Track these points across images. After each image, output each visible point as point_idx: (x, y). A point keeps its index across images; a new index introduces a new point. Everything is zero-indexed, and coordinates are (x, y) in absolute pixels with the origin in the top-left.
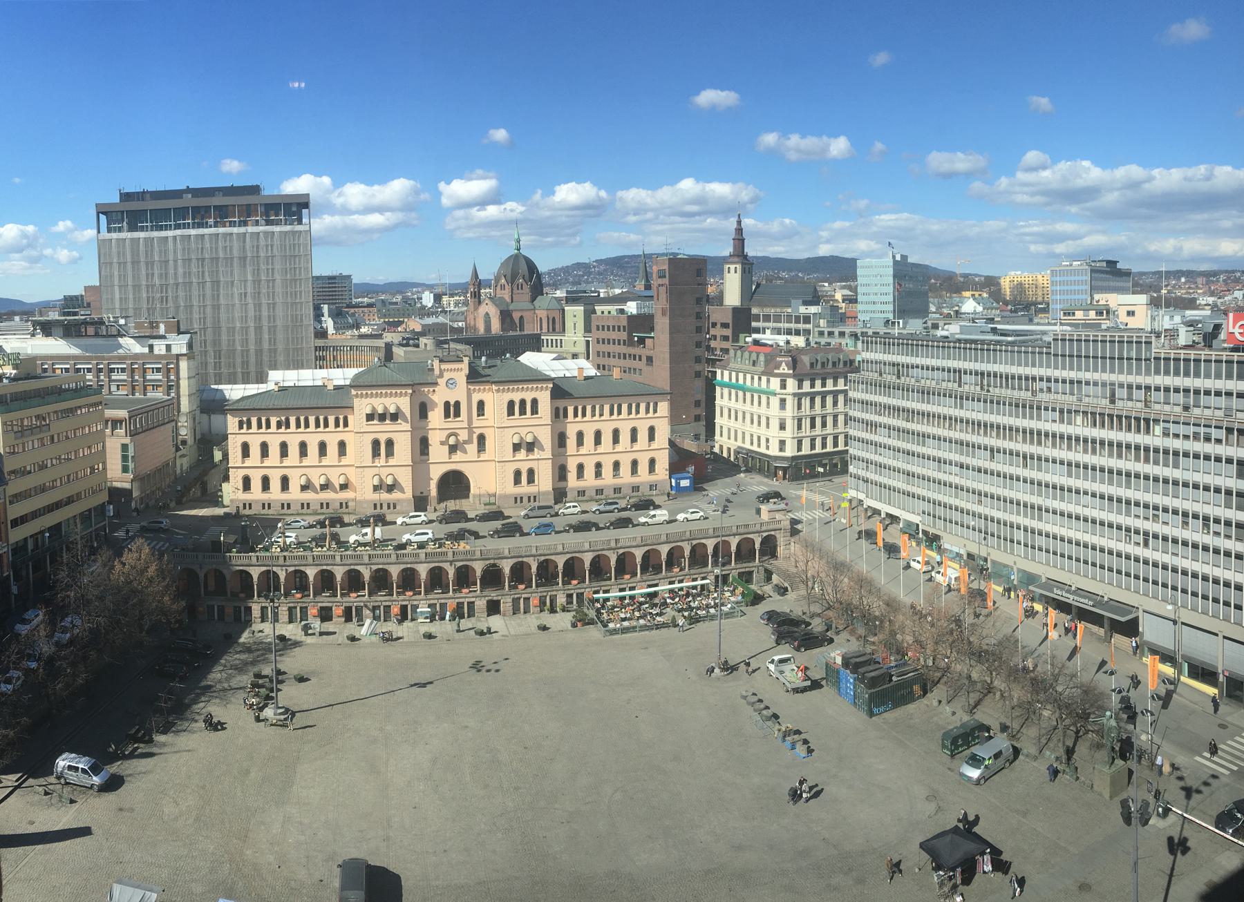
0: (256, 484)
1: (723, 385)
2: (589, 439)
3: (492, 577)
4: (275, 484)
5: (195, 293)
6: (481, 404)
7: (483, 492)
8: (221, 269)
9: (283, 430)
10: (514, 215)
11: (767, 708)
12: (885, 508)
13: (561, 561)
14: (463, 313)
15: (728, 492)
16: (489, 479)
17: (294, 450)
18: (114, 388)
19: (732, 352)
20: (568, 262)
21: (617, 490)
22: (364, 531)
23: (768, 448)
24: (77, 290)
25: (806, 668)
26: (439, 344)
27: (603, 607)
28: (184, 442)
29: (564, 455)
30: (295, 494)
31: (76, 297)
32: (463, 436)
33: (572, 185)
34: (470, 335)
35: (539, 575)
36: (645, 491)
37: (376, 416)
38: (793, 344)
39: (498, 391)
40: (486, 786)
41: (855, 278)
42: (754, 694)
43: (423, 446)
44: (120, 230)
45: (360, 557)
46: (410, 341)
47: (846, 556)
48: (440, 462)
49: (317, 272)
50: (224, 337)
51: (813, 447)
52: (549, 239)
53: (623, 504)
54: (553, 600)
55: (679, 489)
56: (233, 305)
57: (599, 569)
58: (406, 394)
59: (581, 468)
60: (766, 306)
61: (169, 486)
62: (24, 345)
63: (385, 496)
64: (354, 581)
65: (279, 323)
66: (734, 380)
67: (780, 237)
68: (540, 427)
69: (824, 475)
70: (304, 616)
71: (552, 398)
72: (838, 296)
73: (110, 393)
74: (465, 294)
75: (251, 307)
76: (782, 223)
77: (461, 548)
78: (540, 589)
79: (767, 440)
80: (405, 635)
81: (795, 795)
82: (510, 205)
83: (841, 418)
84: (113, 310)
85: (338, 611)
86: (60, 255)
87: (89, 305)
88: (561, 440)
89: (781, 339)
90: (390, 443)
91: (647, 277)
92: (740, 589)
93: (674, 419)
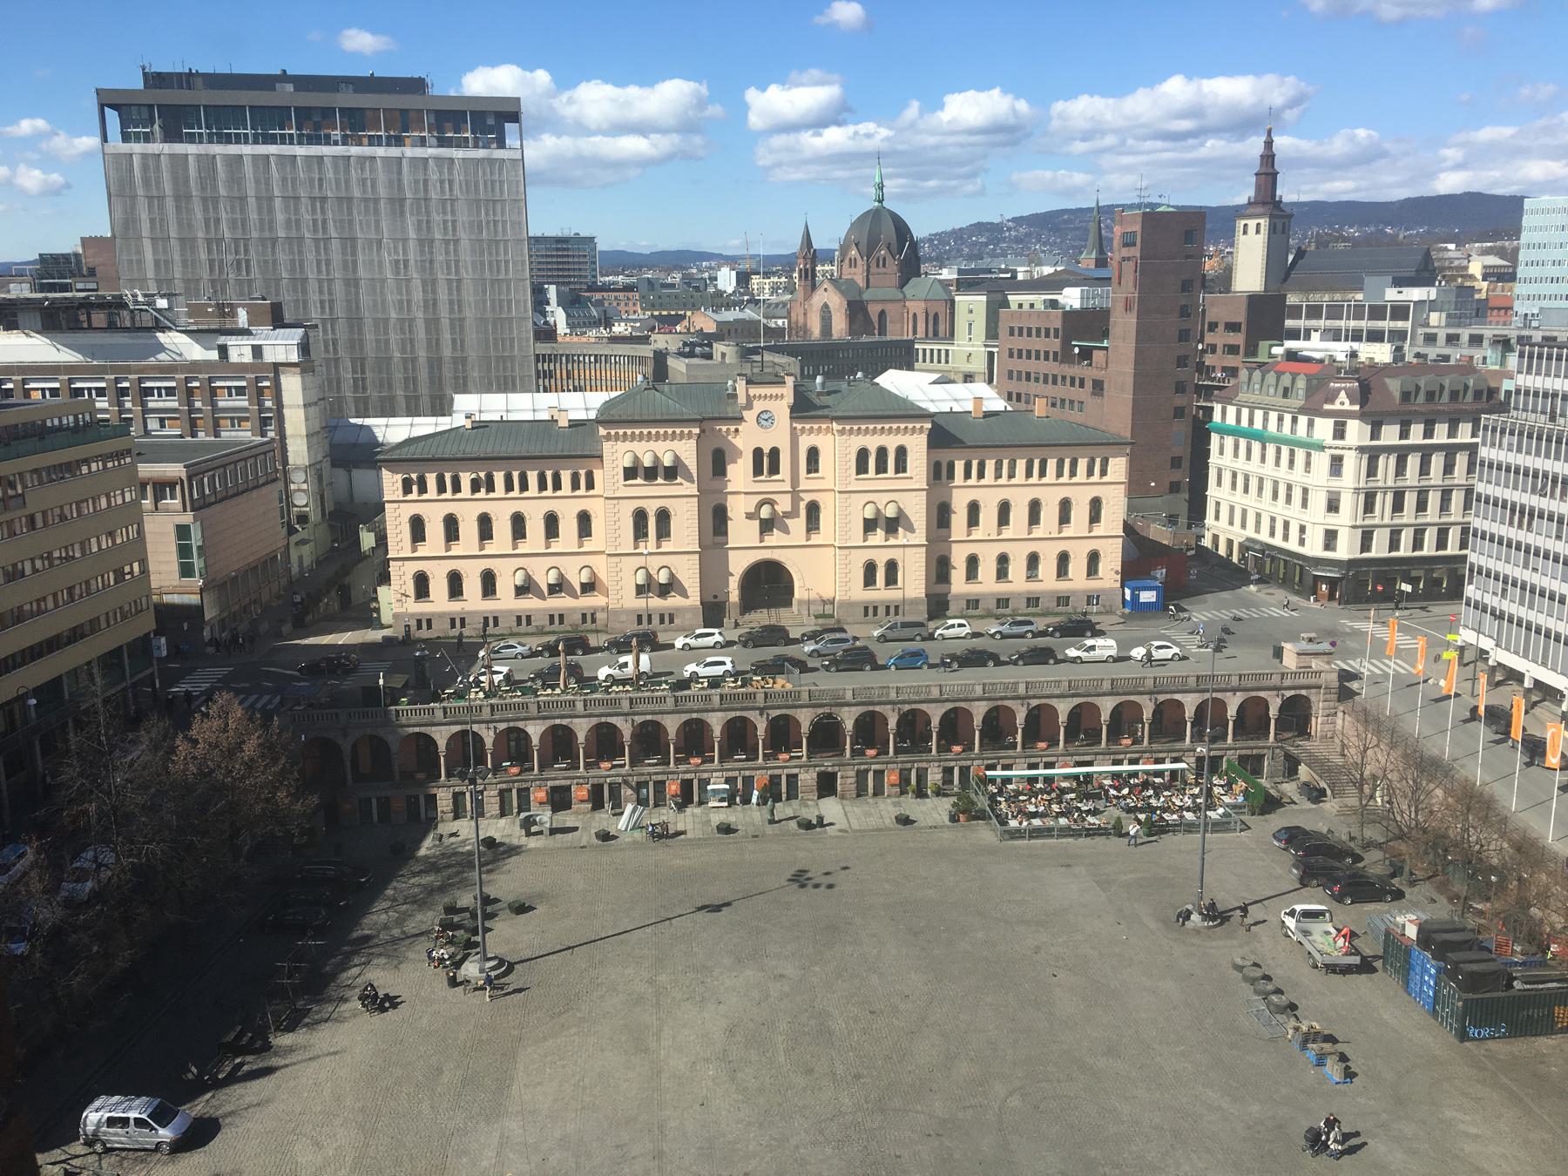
1: (1224, 431)
2: (989, 516)
3: (826, 736)
4: (472, 586)
5: (310, 256)
6: (813, 454)
7: (813, 596)
8: (357, 218)
9: (482, 494)
11: (1279, 991)
13: (936, 714)
14: (784, 304)
15: (1225, 615)
16: (824, 574)
17: (502, 528)
18: (153, 425)
19: (1243, 374)
21: (1033, 601)
22: (622, 660)
23: (1302, 542)
24: (67, 244)
25: (1353, 935)
26: (745, 354)
27: (1000, 793)
28: (303, 519)
29: (946, 540)
30: (506, 600)
31: (66, 257)
32: (784, 504)
33: (971, 93)
34: (797, 341)
35: (900, 736)
37: (641, 472)
38: (1362, 357)
39: (842, 432)
41: (1516, 232)
43: (716, 520)
44: (147, 138)
45: (616, 702)
46: (698, 347)
47: (1445, 747)
48: (745, 546)
49: (535, 230)
50: (369, 336)
52: (932, 183)
53: (1040, 624)
56: (383, 281)
57: (997, 729)
58: (690, 435)
59: (973, 562)
60: (1315, 290)
63: (656, 602)
64: (605, 742)
66: (1245, 423)
67: (1335, 164)
70: (524, 804)
71: (929, 447)
72: (1475, 268)
73: (147, 433)
77: (778, 687)
78: (901, 758)
79: (1302, 529)
80: (689, 827)
81: (1316, 1141)
83: (1457, 498)
84: (142, 283)
85: (580, 792)
88: (941, 515)
89: (1340, 350)
90: (664, 516)
92: (1241, 785)
93: (1136, 487)
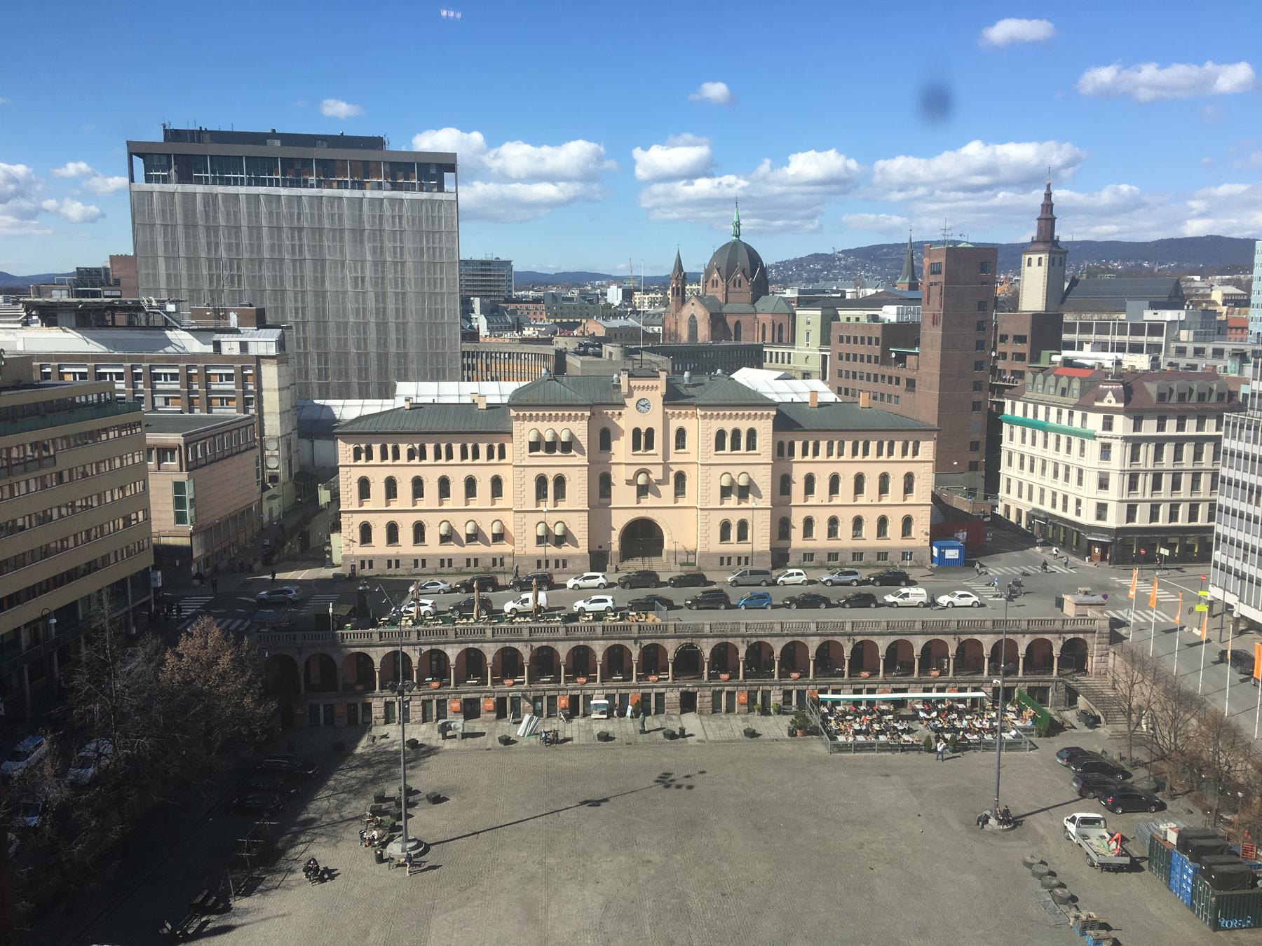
0: (379, 535)
1: (1013, 422)
2: (822, 486)
3: (688, 662)
4: (406, 534)
5: (288, 273)
6: (681, 434)
7: (679, 548)
9: (416, 461)
10: (732, 192)
11: (1062, 886)
13: (778, 646)
14: (660, 315)
16: (688, 530)
17: (431, 489)
18: (159, 402)
19: (1029, 376)
21: (858, 555)
22: (524, 596)
23: (1078, 513)
24: (99, 260)
26: (628, 353)
27: (831, 713)
28: (274, 478)
31: (97, 271)
32: (657, 473)
34: (670, 343)
36: (896, 562)
37: (543, 445)
38: (1126, 365)
39: (704, 417)
41: (1249, 268)
42: (1042, 862)
43: (602, 486)
44: (165, 180)
45: (519, 630)
46: (591, 347)
48: (625, 507)
50: (332, 335)
51: (1154, 516)
52: (779, 223)
53: (863, 574)
54: (766, 697)
55: (942, 562)
56: (345, 293)
58: (583, 417)
59: (809, 523)
61: (253, 540)
62: (10, 338)
63: (552, 550)
64: (509, 664)
66: (1030, 415)
68: (757, 467)
73: (154, 409)
76: (1117, 192)
77: (649, 621)
78: (749, 682)
79: (1078, 502)
82: (728, 179)
84: (156, 291)
86: (83, 214)
87: (117, 283)
88: (783, 484)
89: (1107, 359)
91: (914, 273)
92: (1030, 711)
93: (942, 466)
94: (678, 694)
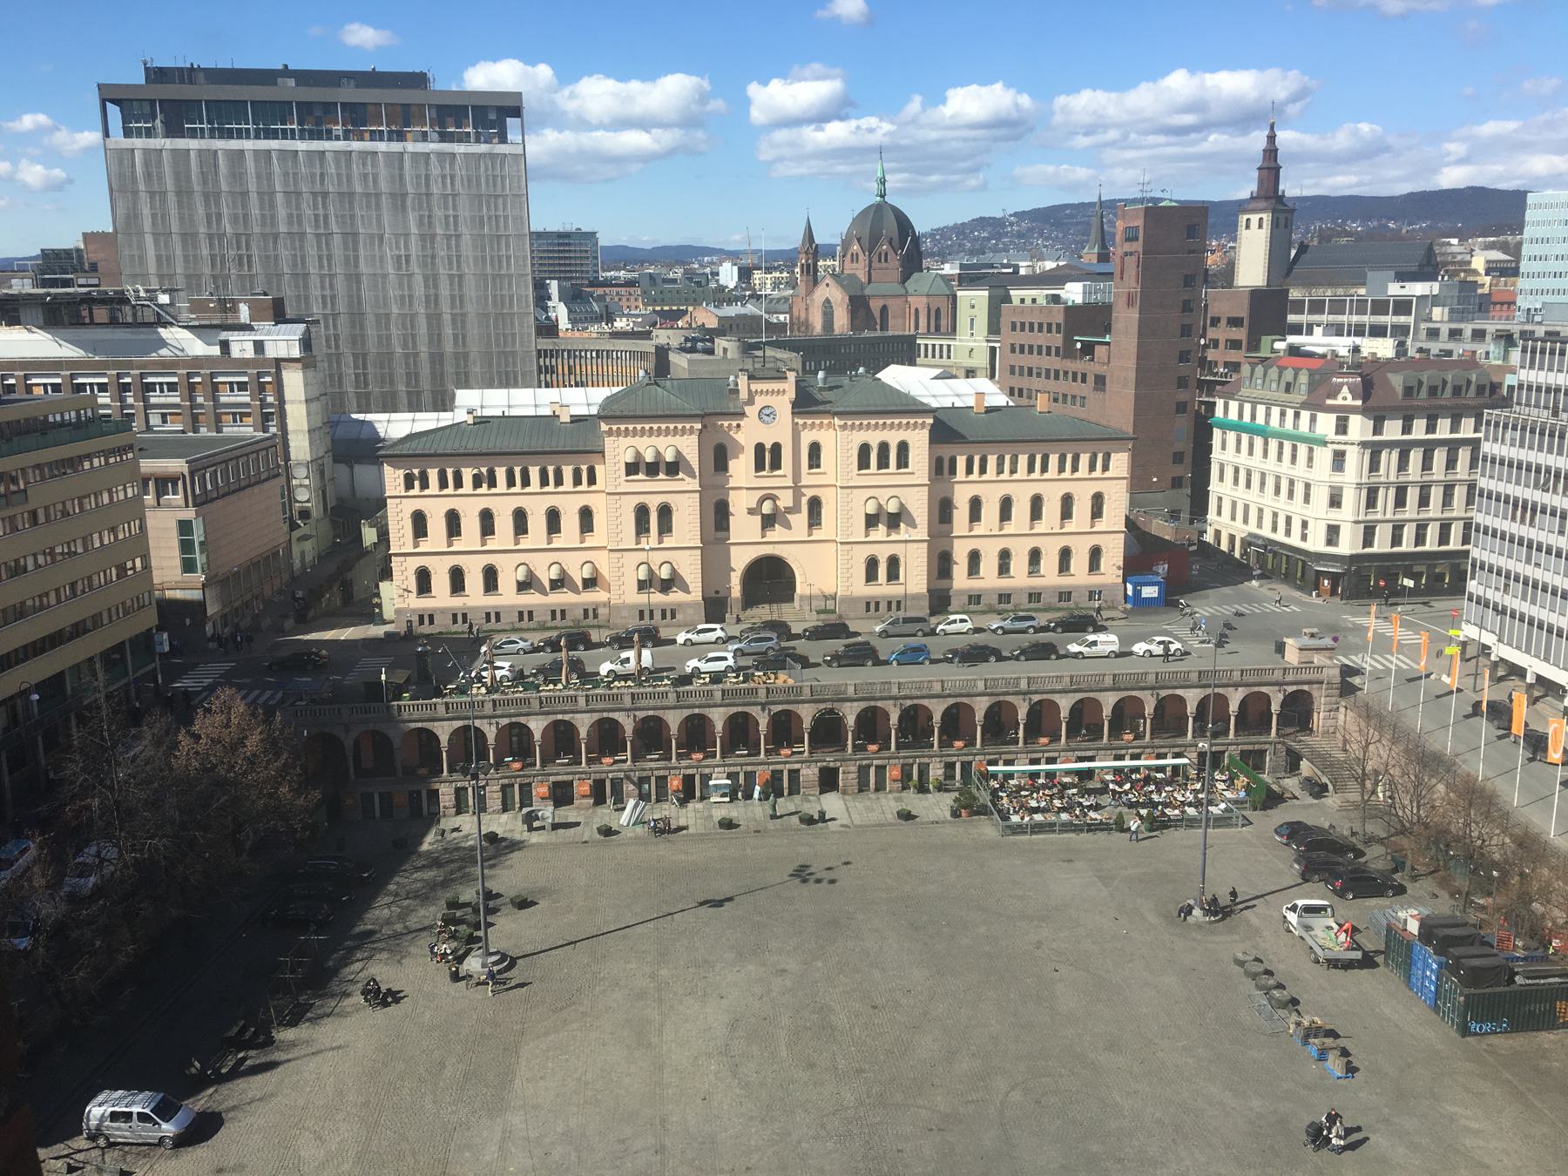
0: (440, 582)
1: (1226, 426)
2: (990, 511)
3: (828, 731)
4: (474, 581)
6: (815, 449)
7: (815, 591)
8: (358, 212)
9: (484, 489)
11: (1280, 986)
12: (1535, 666)
13: (938, 709)
14: (786, 299)
15: (1227, 611)
16: (826, 570)
18: (155, 420)
20: (966, 218)
21: (1035, 596)
22: (624, 655)
23: (1304, 537)
24: (69, 240)
25: (1355, 930)
26: (747, 349)
27: (1002, 786)
28: (305, 514)
29: (948, 535)
31: (67, 252)
32: (785, 500)
34: (798, 335)
35: (901, 730)
36: (1081, 602)
37: (643, 467)
38: (1365, 352)
39: (844, 427)
40: (812, 1066)
42: (1257, 960)
43: (718, 516)
44: (149, 133)
46: (700, 342)
47: (1446, 743)
48: (747, 542)
50: (371, 332)
51: (1396, 540)
52: (934, 178)
53: (1042, 619)
56: (385, 276)
57: (999, 725)
58: (692, 431)
59: (974, 557)
63: (657, 598)
64: (607, 738)
65: (470, 309)
66: (1247, 418)
69: (1412, 592)
71: (931, 442)
73: (149, 428)
74: (790, 268)
75: (418, 280)
77: (780, 682)
79: (1305, 524)
80: (691, 822)
81: (1318, 1136)
83: (1460, 493)
84: (143, 277)
87: (94, 268)
88: (943, 511)
89: (1342, 345)
90: (665, 512)
91: (1104, 241)
92: (1242, 780)
93: (1138, 483)
94: (816, 771)
